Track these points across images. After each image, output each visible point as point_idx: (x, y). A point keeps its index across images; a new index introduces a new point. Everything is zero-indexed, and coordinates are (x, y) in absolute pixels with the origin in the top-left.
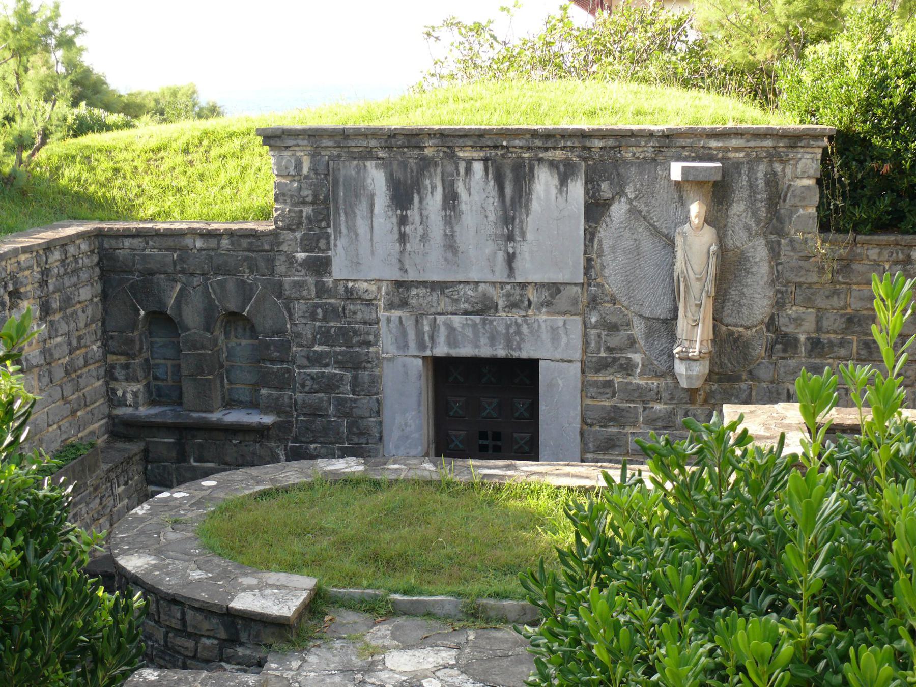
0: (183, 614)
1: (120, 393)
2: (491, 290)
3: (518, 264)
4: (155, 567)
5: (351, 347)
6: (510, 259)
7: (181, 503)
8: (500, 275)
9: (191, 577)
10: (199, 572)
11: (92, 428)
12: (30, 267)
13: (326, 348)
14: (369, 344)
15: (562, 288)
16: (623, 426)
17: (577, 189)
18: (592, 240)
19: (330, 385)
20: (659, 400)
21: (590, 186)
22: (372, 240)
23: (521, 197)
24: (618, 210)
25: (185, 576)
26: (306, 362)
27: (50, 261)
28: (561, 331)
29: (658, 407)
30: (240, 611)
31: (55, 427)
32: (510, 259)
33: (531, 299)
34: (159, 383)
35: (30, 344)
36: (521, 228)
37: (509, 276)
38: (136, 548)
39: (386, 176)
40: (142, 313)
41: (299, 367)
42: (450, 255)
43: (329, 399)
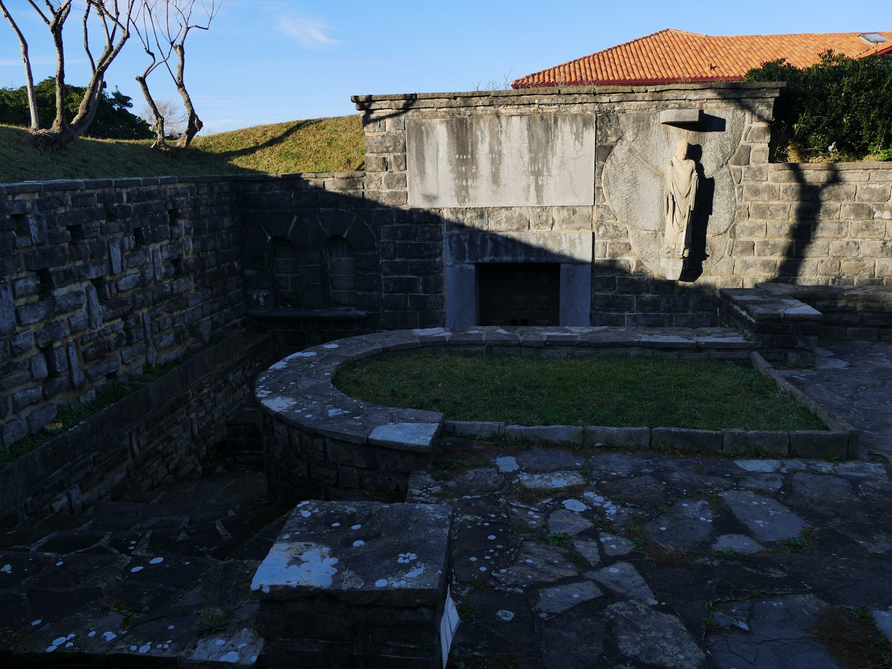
0: (325, 446)
1: (255, 297)
2: (524, 212)
3: (545, 193)
4: (296, 407)
5: (423, 258)
6: (539, 189)
7: (310, 361)
8: (533, 202)
9: (334, 414)
10: (336, 410)
11: (235, 321)
12: (185, 194)
13: (403, 259)
14: (436, 256)
15: (577, 209)
16: (623, 311)
17: (590, 136)
18: (600, 174)
19: (410, 286)
20: (648, 292)
21: (599, 133)
22: (437, 178)
23: (548, 142)
24: (620, 152)
25: (324, 413)
26: (388, 270)
27: (201, 192)
28: (578, 241)
29: (648, 296)
30: (380, 441)
31: (208, 318)
32: (539, 189)
33: (555, 218)
34: (282, 290)
35: (187, 254)
36: (547, 166)
37: (538, 202)
38: (275, 392)
39: (447, 128)
40: (269, 238)
41: (385, 274)
42: (495, 188)
43: (406, 297)
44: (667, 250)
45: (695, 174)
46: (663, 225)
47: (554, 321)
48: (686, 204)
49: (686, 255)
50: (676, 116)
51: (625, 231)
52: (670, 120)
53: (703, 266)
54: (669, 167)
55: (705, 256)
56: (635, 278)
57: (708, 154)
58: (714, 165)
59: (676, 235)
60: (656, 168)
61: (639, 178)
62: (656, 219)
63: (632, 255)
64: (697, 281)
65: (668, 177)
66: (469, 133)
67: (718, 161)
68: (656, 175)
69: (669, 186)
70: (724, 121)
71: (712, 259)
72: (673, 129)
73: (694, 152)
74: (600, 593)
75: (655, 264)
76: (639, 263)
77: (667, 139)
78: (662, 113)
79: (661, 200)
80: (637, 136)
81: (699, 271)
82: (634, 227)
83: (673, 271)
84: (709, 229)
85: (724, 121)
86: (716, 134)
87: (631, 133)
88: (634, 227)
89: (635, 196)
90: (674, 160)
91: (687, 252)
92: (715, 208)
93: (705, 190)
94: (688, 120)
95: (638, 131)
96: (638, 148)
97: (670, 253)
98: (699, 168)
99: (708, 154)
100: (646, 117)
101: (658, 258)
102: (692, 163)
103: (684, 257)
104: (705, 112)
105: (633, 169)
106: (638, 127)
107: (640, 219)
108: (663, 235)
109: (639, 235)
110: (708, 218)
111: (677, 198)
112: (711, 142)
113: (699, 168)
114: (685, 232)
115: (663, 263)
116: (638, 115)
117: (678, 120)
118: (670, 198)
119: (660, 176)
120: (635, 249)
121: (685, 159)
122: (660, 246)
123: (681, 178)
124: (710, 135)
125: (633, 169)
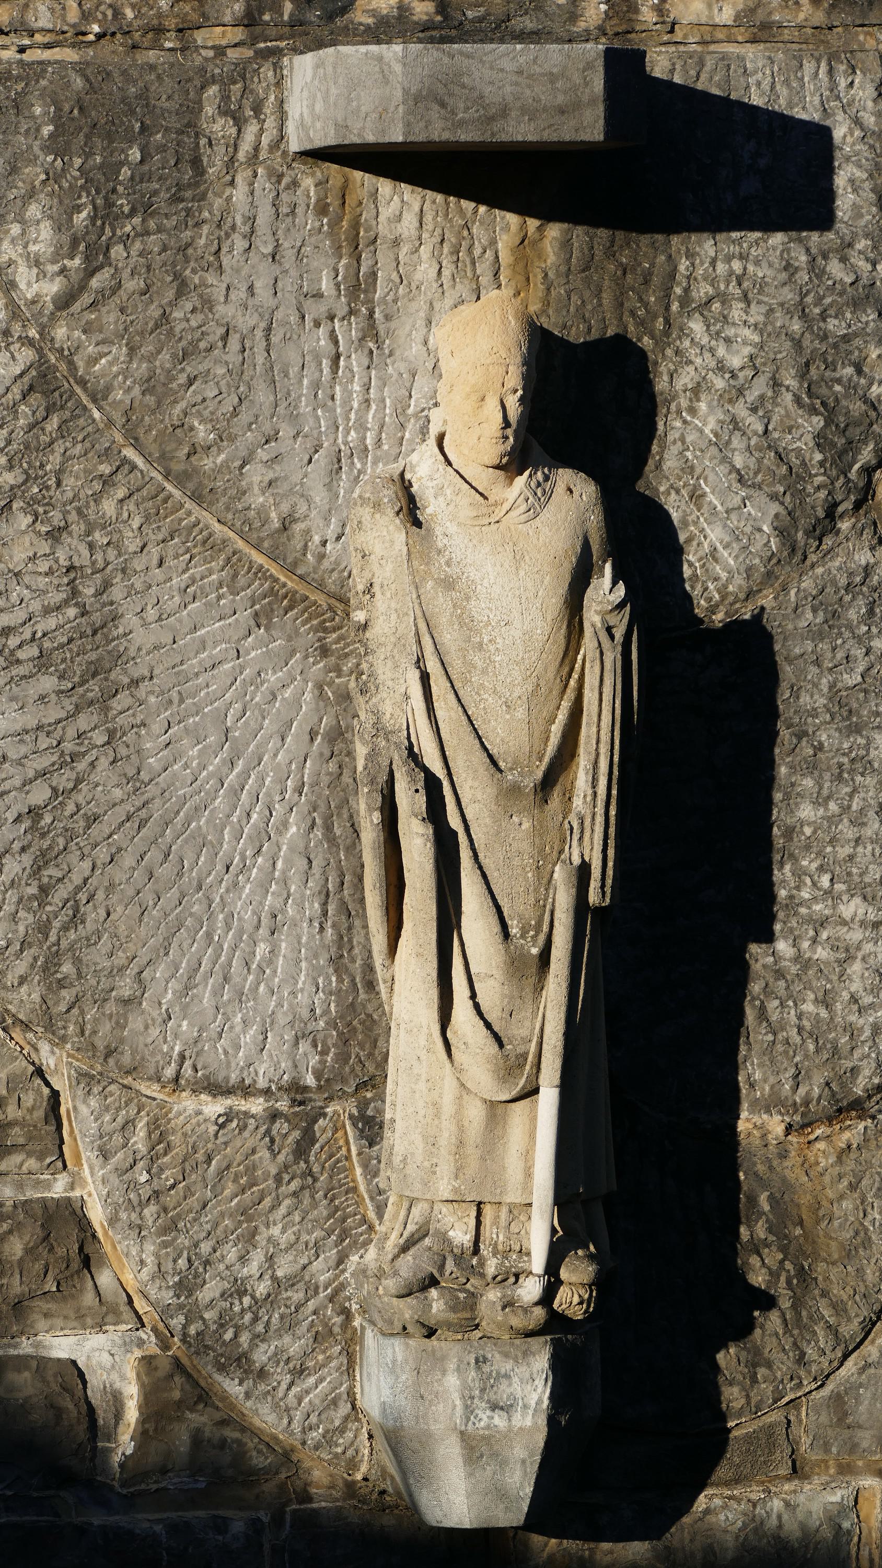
44: (410, 1266)
45: (605, 591)
46: (356, 1045)
47: (109, 1442)
48: (541, 862)
49: (570, 1300)
50: (419, 100)
51: (33, 1097)
52: (368, 133)
53: (732, 1396)
54: (383, 536)
55: (739, 1308)
56: (147, 1521)
57: (708, 419)
58: (763, 514)
59: (472, 1129)
60: (280, 538)
61: (138, 632)
62: (297, 983)
63: (103, 1316)
64: (682, 1531)
65: (386, 619)
66: (357, 923)
67: (795, 477)
68: (272, 606)
69: (394, 696)
70: (818, 140)
71: (798, 1325)
72: (399, 209)
73: (584, 410)
74: (797, 337)
75: (317, 1388)
76: (179, 1383)
77: (359, 288)
78: (303, 68)
79: (332, 822)
80: (96, 256)
81: (697, 1445)
82: (109, 1065)
83: (477, 1449)
84: (755, 1072)
85: (810, 146)
86: (766, 253)
87: (44, 237)
88: (109, 1065)
89: (106, 785)
90: (424, 467)
91: (577, 1273)
92: (796, 881)
93: (697, 730)
94: (520, 131)
95: (106, 214)
96: (106, 363)
97: (445, 1289)
98: (638, 541)
99: (708, 419)
100: (165, 98)
101: (341, 1342)
102: (571, 502)
103: (555, 1323)
104: (660, 64)
105: (73, 549)
106: (101, 182)
107: (164, 989)
108: (371, 1128)
109: (159, 1135)
110: (740, 973)
111: (474, 798)
112: (726, 323)
113: (638, 541)
114: (548, 1099)
115: (384, 1377)
116: (96, 76)
117: (436, 130)
118: (410, 800)
119: (315, 609)
120: (130, 1265)
121: (514, 463)
122: (348, 1233)
123: (482, 598)
124: (710, 259)
125: (73, 549)
